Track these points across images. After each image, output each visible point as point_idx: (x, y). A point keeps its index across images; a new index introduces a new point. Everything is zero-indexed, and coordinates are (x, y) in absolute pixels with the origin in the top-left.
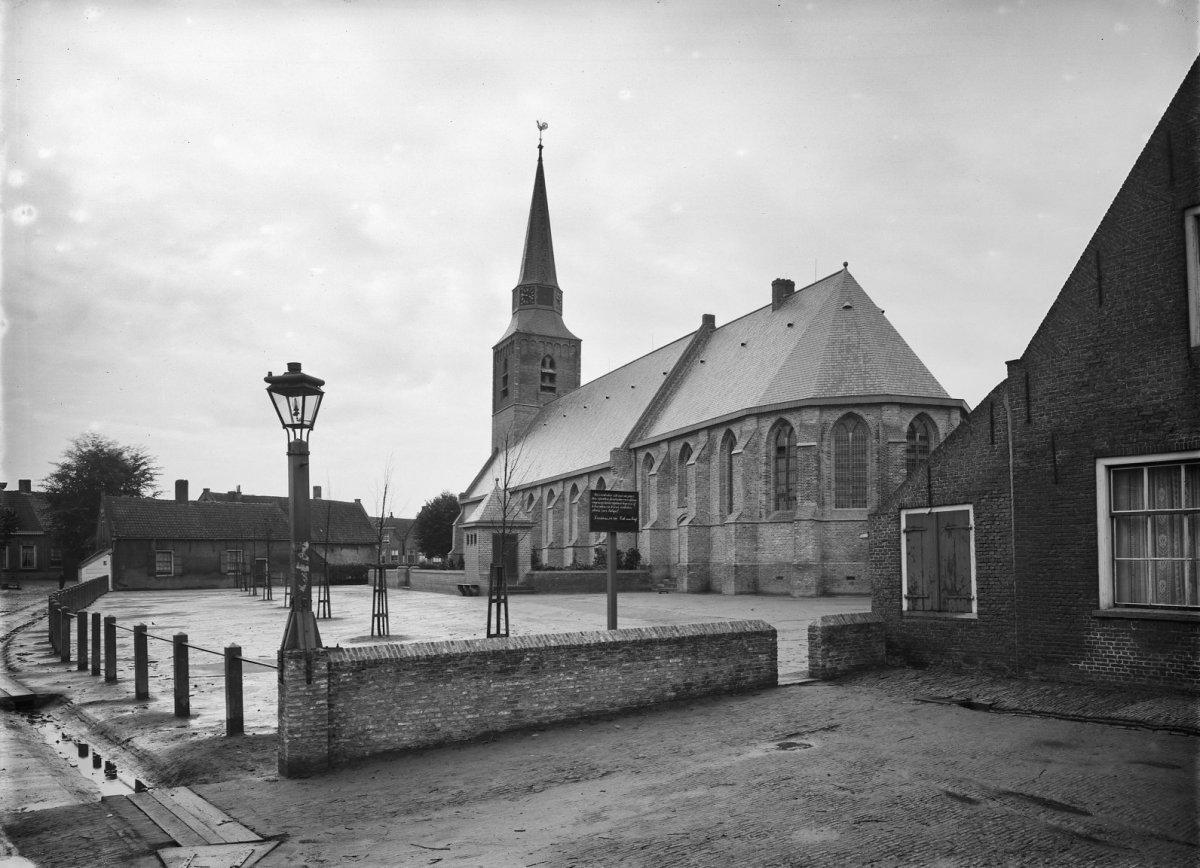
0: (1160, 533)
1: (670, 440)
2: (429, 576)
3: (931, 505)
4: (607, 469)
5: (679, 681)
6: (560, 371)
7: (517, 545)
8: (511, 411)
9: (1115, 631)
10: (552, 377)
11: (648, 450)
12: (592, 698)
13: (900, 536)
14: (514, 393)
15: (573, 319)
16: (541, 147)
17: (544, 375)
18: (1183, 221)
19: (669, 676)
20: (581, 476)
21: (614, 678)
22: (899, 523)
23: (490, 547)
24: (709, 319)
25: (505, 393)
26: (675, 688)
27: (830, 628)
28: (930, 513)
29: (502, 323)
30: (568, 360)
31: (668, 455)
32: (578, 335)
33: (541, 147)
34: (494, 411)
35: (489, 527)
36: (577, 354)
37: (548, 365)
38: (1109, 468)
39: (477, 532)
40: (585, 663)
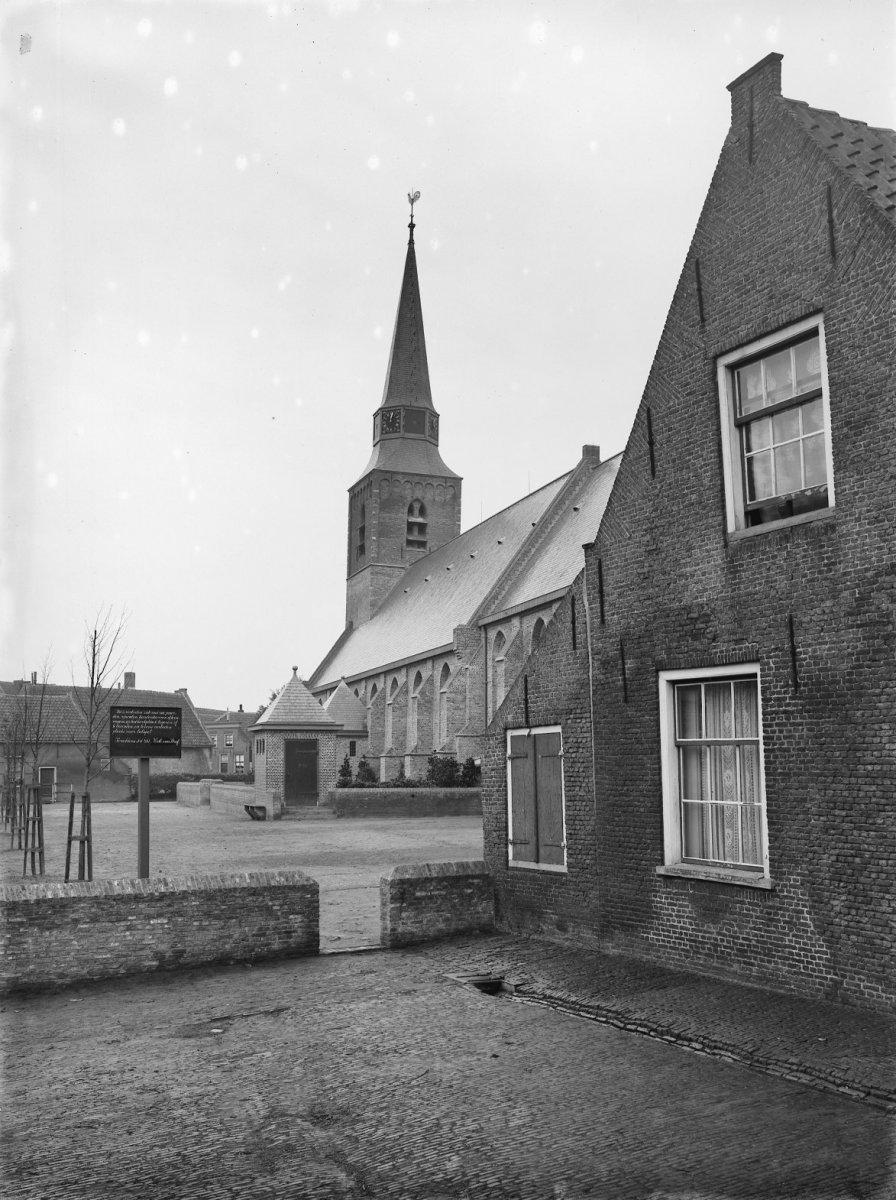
0: (726, 768)
1: (522, 614)
2: (226, 792)
3: (529, 727)
4: (450, 653)
5: (163, 947)
6: (432, 519)
7: (317, 754)
8: (367, 573)
9: (675, 894)
10: (422, 527)
11: (499, 628)
12: (31, 967)
13: (505, 763)
14: (371, 551)
15: (453, 450)
16: (412, 226)
17: (410, 526)
18: (714, 373)
19: (149, 940)
20: (424, 661)
21: (67, 942)
22: (506, 751)
23: (282, 756)
24: (591, 452)
25: (362, 549)
26: (159, 956)
27: (402, 882)
28: (529, 735)
29: (359, 456)
30: (444, 504)
31: (519, 635)
32: (457, 471)
33: (412, 226)
34: (349, 573)
35: (281, 731)
36: (456, 498)
37: (416, 512)
38: (672, 683)
39: (265, 736)
40: (21, 924)
